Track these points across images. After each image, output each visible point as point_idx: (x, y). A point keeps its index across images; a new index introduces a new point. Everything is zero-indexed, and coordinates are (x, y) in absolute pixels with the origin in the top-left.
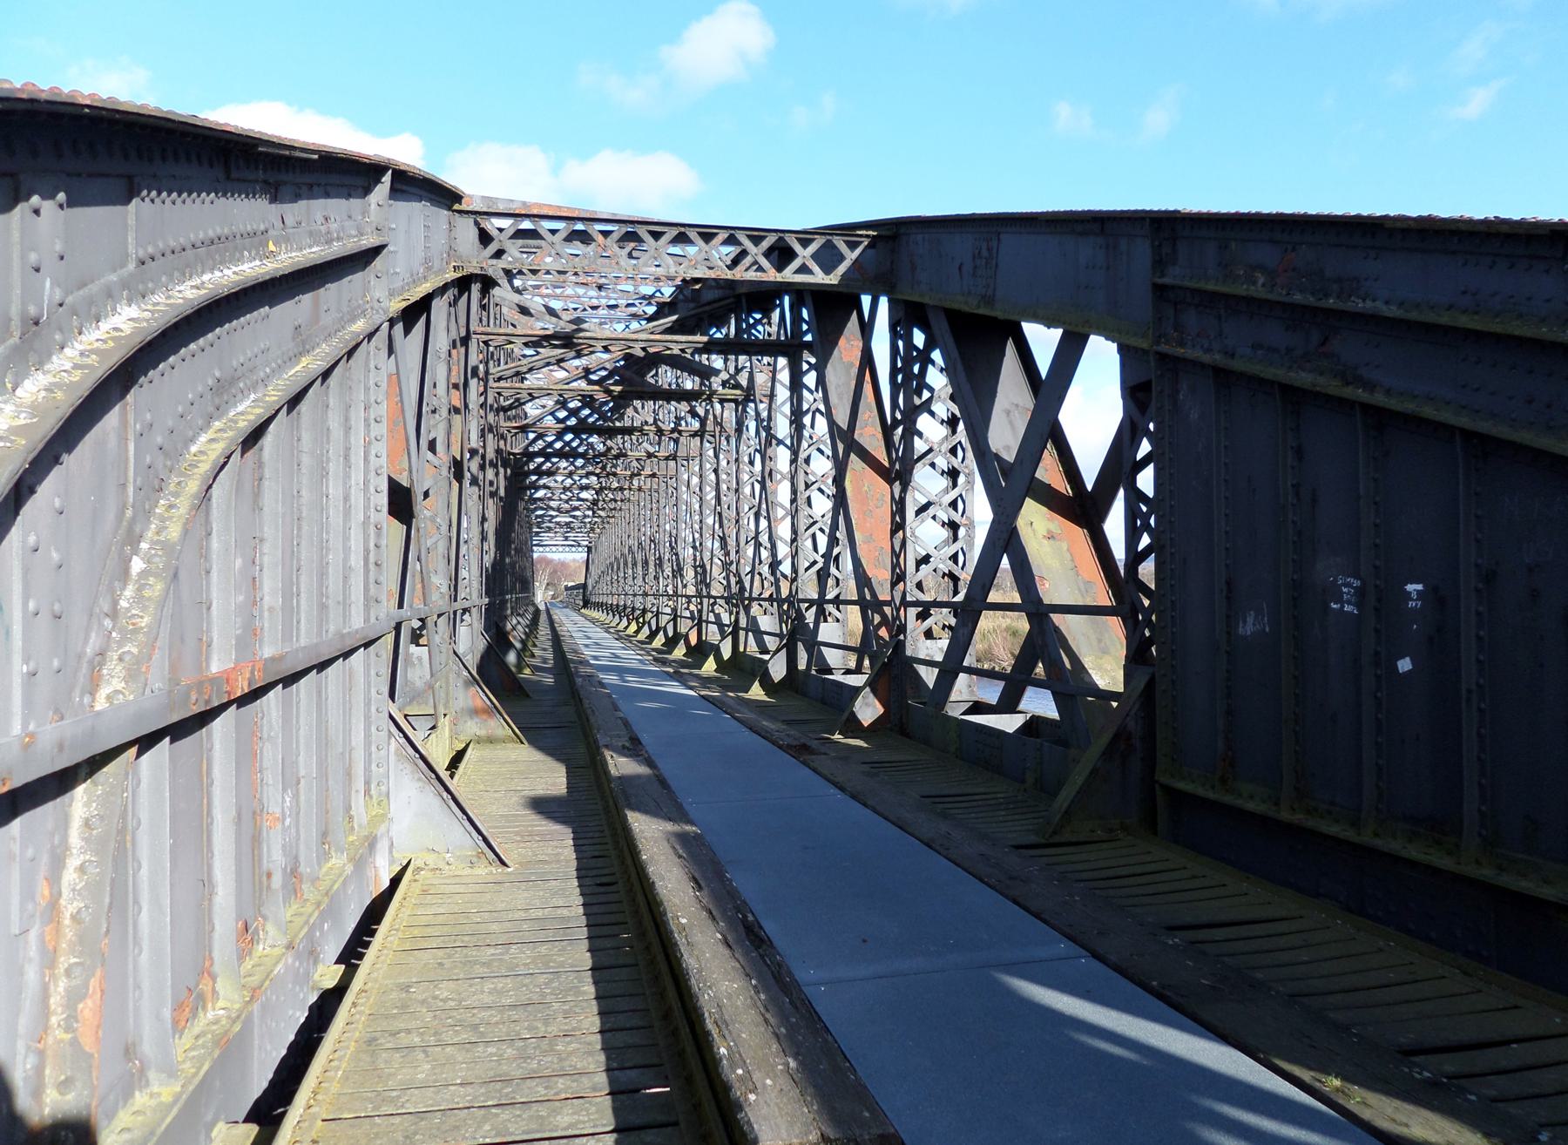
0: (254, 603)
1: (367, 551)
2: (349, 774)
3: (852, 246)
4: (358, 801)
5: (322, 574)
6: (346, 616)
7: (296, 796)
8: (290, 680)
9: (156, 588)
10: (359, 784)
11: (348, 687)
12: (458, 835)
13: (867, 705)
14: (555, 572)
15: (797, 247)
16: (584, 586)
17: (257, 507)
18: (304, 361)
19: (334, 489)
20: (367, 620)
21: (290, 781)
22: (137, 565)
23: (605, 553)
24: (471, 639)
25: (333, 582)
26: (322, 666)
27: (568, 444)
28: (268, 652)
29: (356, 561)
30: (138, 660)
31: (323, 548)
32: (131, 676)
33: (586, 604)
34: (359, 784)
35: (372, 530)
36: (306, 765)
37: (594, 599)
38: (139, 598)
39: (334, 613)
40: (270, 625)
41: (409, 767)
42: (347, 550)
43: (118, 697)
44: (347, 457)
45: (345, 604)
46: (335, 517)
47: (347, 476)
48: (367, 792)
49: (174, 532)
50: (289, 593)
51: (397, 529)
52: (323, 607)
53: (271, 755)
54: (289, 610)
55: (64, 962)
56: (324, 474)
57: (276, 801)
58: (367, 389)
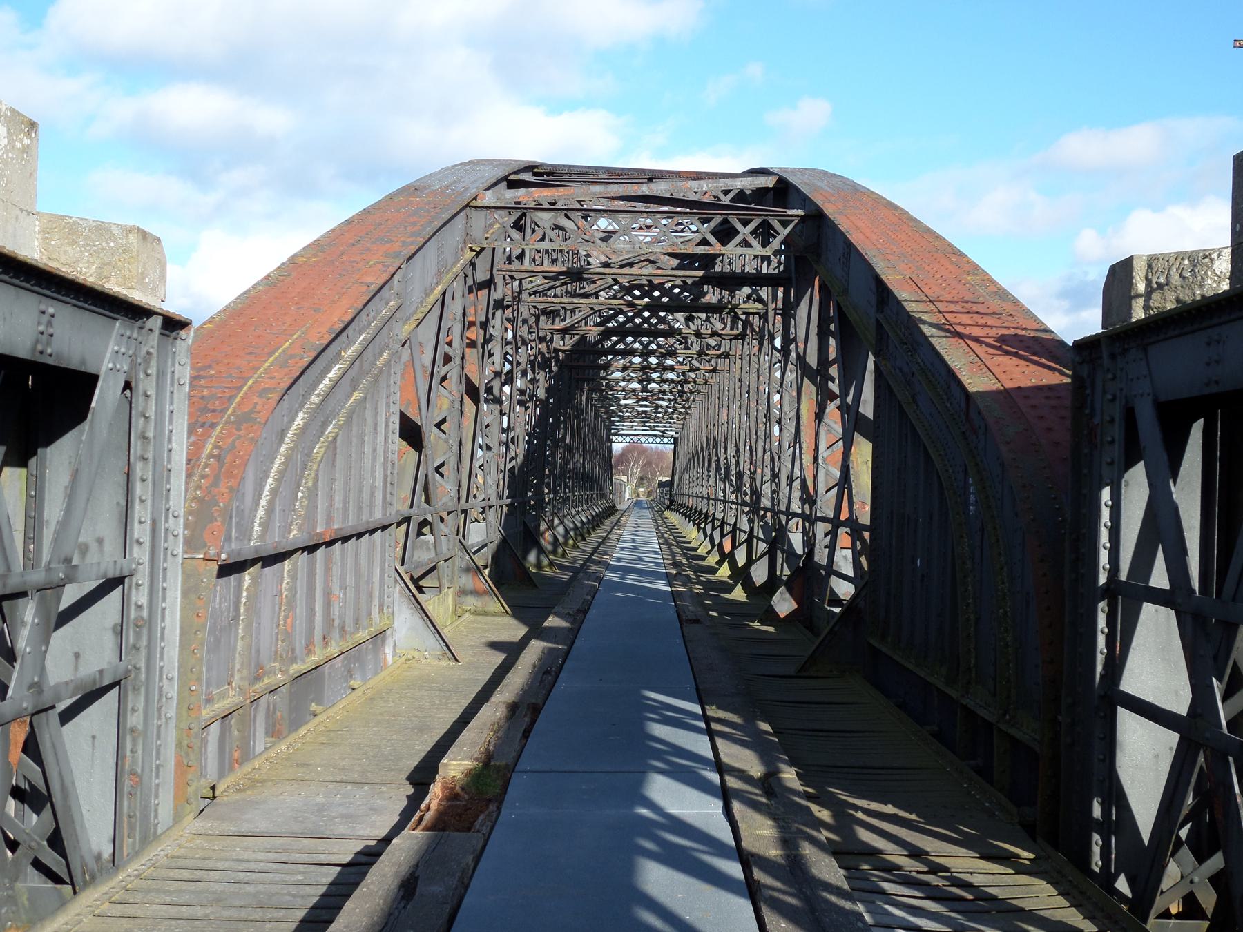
0: (331, 505)
1: (385, 477)
2: (371, 596)
3: (784, 224)
4: (375, 611)
5: (360, 492)
6: (371, 513)
7: (345, 594)
8: (345, 539)
9: (305, 503)
10: (376, 601)
11: (371, 550)
12: (432, 641)
13: (784, 600)
14: (649, 464)
15: (739, 226)
16: (670, 484)
17: (334, 465)
18: (355, 394)
19: (367, 449)
20: (384, 514)
21: (343, 587)
22: (300, 495)
23: (687, 448)
24: (483, 533)
25: (366, 495)
26: (359, 536)
27: (646, 320)
28: (336, 527)
29: (379, 483)
30: (302, 524)
31: (362, 478)
32: (299, 530)
33: (673, 505)
34: (376, 601)
35: (389, 465)
36: (350, 581)
37: (678, 499)
38: (301, 506)
39: (366, 510)
40: (337, 516)
41: (406, 601)
42: (374, 477)
43: (296, 536)
44: (375, 429)
45: (372, 506)
46: (368, 462)
47: (375, 438)
48: (381, 610)
49: (310, 484)
50: (345, 501)
51: (412, 454)
52: (360, 508)
53: (336, 570)
54: (345, 510)
55: (284, 608)
56: (363, 441)
57: (336, 590)
58: (388, 386)
